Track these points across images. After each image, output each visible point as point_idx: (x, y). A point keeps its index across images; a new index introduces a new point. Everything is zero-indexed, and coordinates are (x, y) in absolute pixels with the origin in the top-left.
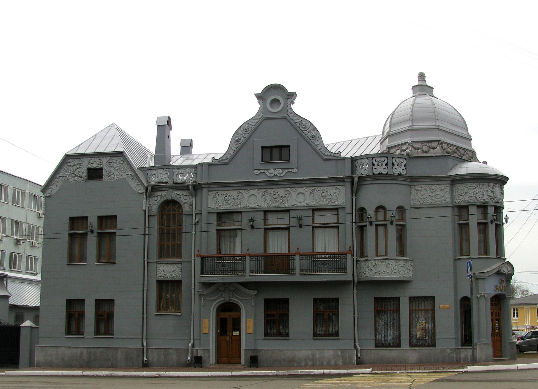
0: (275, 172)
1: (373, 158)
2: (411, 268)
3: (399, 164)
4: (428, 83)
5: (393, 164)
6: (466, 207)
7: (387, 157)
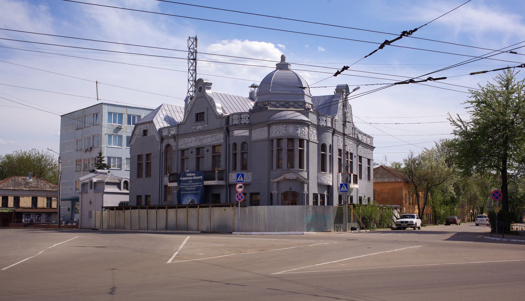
0: (199, 127)
2: (251, 177)
3: (245, 118)
4: (286, 61)
6: (282, 139)
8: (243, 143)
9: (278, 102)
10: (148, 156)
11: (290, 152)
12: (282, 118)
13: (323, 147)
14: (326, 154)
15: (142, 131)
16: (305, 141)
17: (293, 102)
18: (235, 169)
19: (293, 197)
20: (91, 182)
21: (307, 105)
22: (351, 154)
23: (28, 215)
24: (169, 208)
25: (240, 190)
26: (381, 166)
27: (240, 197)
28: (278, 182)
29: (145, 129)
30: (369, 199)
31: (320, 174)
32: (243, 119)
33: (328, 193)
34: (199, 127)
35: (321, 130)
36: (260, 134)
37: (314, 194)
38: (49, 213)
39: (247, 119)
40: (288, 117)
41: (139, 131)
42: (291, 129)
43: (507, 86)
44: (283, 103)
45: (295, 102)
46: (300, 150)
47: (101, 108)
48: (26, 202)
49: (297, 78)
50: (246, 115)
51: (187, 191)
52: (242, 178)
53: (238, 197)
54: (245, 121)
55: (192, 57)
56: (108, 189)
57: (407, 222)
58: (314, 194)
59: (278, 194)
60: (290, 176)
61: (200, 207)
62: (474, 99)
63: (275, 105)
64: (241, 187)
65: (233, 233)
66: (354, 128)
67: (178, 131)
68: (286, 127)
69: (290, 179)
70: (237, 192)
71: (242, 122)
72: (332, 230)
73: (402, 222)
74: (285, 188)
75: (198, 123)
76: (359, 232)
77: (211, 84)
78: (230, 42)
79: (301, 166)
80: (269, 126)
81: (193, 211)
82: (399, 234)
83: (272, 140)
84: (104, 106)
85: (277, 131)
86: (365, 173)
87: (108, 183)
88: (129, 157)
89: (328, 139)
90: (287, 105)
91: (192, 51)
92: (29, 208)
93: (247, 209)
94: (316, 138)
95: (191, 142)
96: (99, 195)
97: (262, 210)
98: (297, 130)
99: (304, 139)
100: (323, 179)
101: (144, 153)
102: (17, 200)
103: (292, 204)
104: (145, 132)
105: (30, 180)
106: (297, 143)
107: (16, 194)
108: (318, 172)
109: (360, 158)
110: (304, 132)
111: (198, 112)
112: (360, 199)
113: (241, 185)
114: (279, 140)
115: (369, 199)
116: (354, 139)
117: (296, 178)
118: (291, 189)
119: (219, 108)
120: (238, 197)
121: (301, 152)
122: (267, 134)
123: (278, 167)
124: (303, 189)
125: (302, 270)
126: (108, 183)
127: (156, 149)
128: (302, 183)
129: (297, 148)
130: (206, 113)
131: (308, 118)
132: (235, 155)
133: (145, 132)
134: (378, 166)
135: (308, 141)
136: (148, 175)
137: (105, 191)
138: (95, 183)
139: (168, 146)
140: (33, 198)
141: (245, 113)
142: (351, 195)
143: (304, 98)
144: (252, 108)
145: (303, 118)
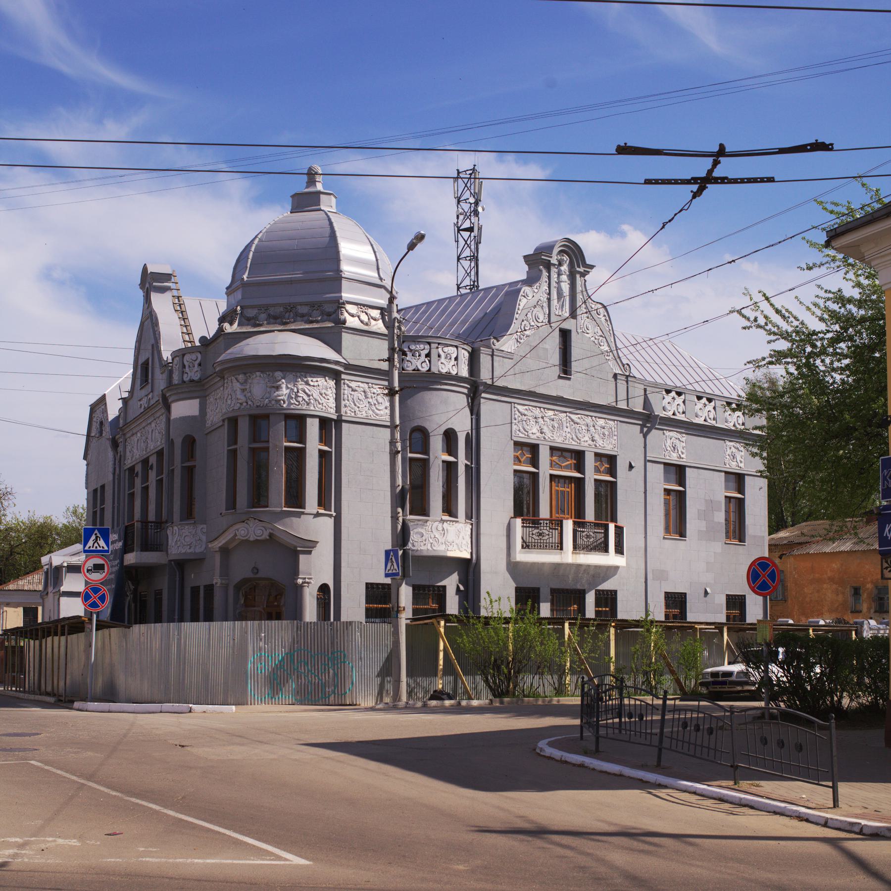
1: (184, 355)
5: (439, 356)
6: (266, 417)
7: (429, 343)
8: (190, 443)
9: (265, 308)
10: (103, 487)
14: (456, 464)
16: (313, 428)
17: (306, 304)
22: (609, 461)
32: (187, 370)
33: (463, 580)
35: (411, 387)
39: (196, 368)
42: (258, 386)
45: (312, 305)
49: (328, 229)
50: (194, 356)
52: (102, 543)
54: (193, 374)
55: (467, 225)
59: (226, 587)
60: (253, 531)
63: (255, 318)
68: (246, 381)
69: (247, 541)
71: (186, 378)
74: (241, 570)
78: (517, 162)
79: (296, 497)
86: (704, 515)
88: (85, 506)
90: (282, 317)
98: (278, 388)
103: (270, 617)
109: (678, 472)
110: (317, 396)
113: (99, 561)
116: (629, 414)
117: (265, 536)
118: (256, 570)
121: (297, 457)
123: (232, 504)
128: (293, 551)
129: (313, 445)
131: (338, 350)
135: (330, 427)
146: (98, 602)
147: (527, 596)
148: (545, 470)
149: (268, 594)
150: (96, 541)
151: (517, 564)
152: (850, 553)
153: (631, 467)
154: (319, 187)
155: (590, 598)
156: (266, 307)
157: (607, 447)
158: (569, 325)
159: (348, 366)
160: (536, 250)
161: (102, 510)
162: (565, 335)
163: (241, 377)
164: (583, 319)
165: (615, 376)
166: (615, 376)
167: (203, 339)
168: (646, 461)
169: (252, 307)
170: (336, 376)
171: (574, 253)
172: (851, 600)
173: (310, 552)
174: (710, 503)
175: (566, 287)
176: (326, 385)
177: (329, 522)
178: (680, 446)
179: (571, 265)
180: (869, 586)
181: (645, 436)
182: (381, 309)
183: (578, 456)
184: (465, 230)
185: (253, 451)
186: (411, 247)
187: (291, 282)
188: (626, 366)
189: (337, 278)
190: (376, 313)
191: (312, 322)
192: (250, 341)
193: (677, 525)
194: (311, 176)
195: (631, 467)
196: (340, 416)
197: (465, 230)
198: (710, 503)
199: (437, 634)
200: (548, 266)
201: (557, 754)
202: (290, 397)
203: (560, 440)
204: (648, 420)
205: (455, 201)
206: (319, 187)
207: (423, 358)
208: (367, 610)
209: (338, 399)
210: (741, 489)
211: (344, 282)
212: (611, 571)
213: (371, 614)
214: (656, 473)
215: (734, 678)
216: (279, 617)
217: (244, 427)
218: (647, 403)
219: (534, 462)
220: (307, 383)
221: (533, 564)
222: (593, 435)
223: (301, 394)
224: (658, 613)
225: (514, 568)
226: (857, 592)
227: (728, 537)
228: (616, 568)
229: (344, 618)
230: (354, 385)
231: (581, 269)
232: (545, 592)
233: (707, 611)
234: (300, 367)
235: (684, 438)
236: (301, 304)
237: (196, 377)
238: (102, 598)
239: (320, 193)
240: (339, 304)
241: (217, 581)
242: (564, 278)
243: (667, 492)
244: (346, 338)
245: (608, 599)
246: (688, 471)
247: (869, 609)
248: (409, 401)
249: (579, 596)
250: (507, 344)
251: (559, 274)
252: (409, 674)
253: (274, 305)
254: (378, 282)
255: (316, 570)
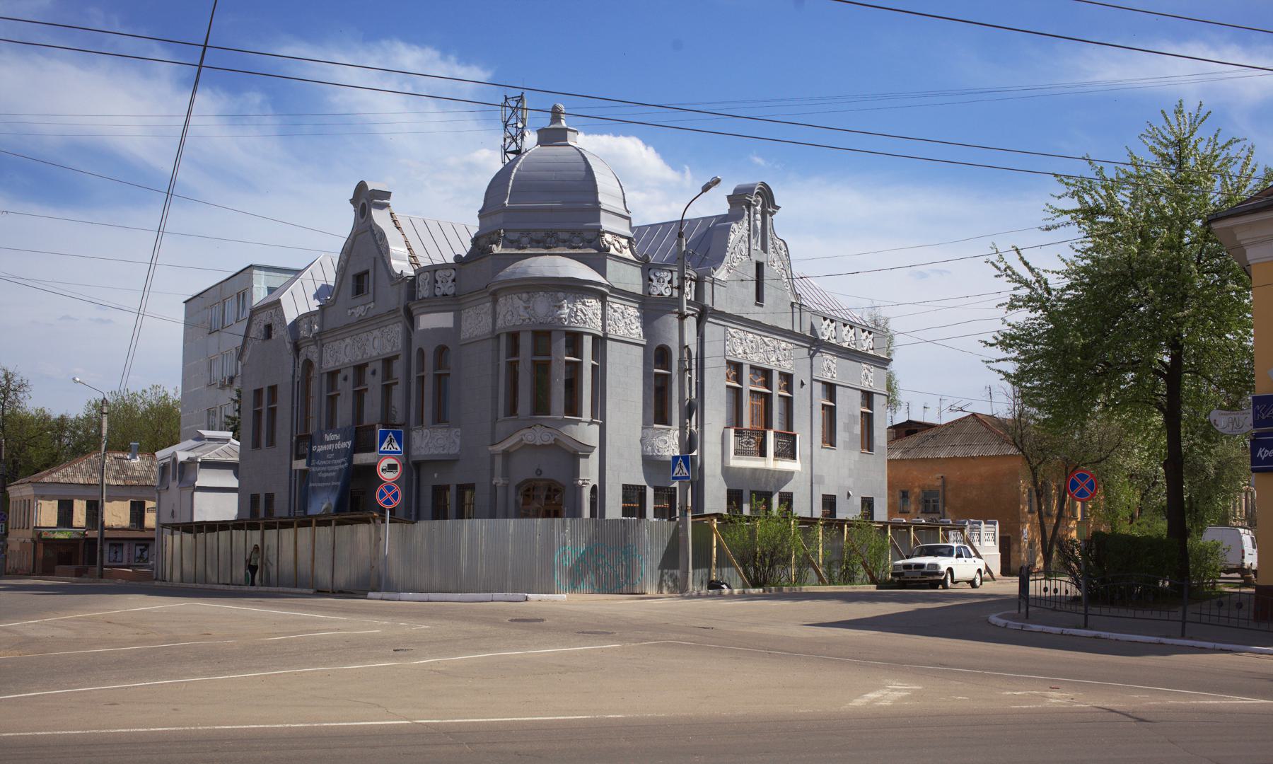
2: (458, 441)
8: (442, 351)
9: (526, 232)
10: (273, 389)
11: (547, 369)
12: (517, 276)
13: (659, 355)
15: (262, 327)
16: (587, 343)
17: (567, 231)
18: (420, 421)
19: (549, 495)
20: (175, 460)
21: (608, 237)
22: (787, 378)
23: (115, 545)
24: (299, 526)
25: (389, 476)
26: (974, 415)
27: (389, 496)
28: (507, 454)
29: (268, 321)
30: (868, 503)
31: (650, 432)
32: (439, 284)
34: (360, 311)
35: (651, 309)
36: (477, 322)
37: (627, 489)
38: (139, 543)
39: (450, 283)
40: (564, 273)
41: (258, 330)
42: (541, 305)
43: (1180, 161)
44: (540, 235)
45: (573, 233)
46: (568, 362)
47: (251, 280)
48: (117, 514)
51: (321, 480)
52: (396, 445)
53: (382, 495)
54: (448, 288)
55: (513, 147)
56: (205, 478)
57: (922, 566)
58: (627, 489)
59: (506, 487)
61: (339, 523)
62: (1074, 204)
63: (518, 241)
64: (392, 467)
65: (371, 594)
66: (797, 306)
67: (321, 325)
69: (534, 446)
70: (381, 481)
71: (438, 292)
72: (651, 591)
73: (907, 567)
74: (524, 470)
75: (359, 300)
76: (743, 596)
77: (387, 195)
79: (573, 407)
80: (495, 297)
81: (324, 533)
82: (807, 602)
83: (498, 337)
84: (255, 272)
85: (513, 312)
86: (848, 428)
87: (207, 465)
89: (680, 334)
90: (548, 241)
91: (513, 131)
92: (123, 529)
93: (423, 526)
94: (640, 330)
95: (341, 354)
96: (187, 493)
97: (475, 533)
98: (560, 307)
99: (582, 334)
100: (661, 445)
101: (265, 386)
102: (94, 510)
104: (269, 328)
105: (133, 461)
106: (560, 344)
107: (93, 494)
108: (646, 425)
109: (830, 389)
110: (587, 315)
111: (358, 270)
112: (829, 502)
113: (393, 462)
114: (514, 337)
115: (868, 503)
117: (551, 441)
118: (539, 472)
119: (399, 258)
120: (382, 495)
121: (574, 371)
122: (490, 320)
124: (576, 473)
125: (1215, 699)
126: (207, 465)
127: (284, 374)
128: (573, 455)
130: (371, 274)
131: (604, 275)
132: (421, 380)
133: (269, 328)
134: (960, 415)
135: (600, 342)
136: (271, 442)
137: (197, 484)
138: (182, 463)
139: (308, 364)
140: (60, 502)
141: (445, 266)
142: (785, 489)
143: (599, 220)
144: (464, 255)
145: (583, 272)
146: (392, 500)
147: (734, 497)
148: (747, 386)
149: (549, 495)
150: (390, 442)
151: (729, 468)
152: (901, 460)
153: (802, 384)
154: (564, 124)
155: (775, 500)
156: (528, 232)
157: (787, 367)
158: (762, 258)
159: (613, 289)
160: (735, 190)
161: (272, 411)
162: (759, 266)
163: (525, 296)
164: (772, 255)
165: (792, 304)
166: (792, 304)
167: (458, 257)
168: (812, 380)
169: (515, 231)
170: (602, 297)
171: (766, 194)
172: (899, 501)
173: (587, 457)
174: (852, 416)
175: (759, 224)
176: (594, 304)
177: (596, 428)
178: (833, 366)
179: (763, 206)
180: (917, 490)
181: (812, 357)
182: (628, 238)
183: (767, 373)
184: (512, 152)
185: (535, 364)
186: (706, 188)
187: (551, 210)
188: (798, 296)
189: (596, 209)
190: (624, 242)
191: (574, 248)
192: (526, 262)
193: (830, 439)
194: (556, 114)
195: (802, 384)
196: (605, 334)
197: (512, 152)
198: (852, 416)
199: (711, 530)
200: (749, 205)
201: (1002, 622)
202: (570, 316)
203: (756, 359)
204: (815, 344)
205: (501, 126)
206: (564, 124)
207: (666, 284)
208: (624, 508)
209: (604, 319)
210: (870, 406)
211: (602, 213)
212: (788, 476)
213: (626, 512)
214: (818, 388)
215: (925, 569)
216: (557, 514)
217: (526, 343)
218: (813, 329)
219: (738, 378)
220: (584, 304)
221: (740, 469)
222: (780, 356)
223: (579, 313)
224: (818, 513)
225: (727, 472)
226: (905, 495)
227: (863, 447)
228: (792, 473)
229: (608, 517)
230: (616, 305)
231: (771, 210)
232: (746, 494)
233: (848, 511)
234: (578, 289)
235: (835, 360)
236: (562, 231)
237: (451, 291)
238: (395, 496)
239: (566, 130)
240: (599, 233)
241: (499, 481)
242: (759, 216)
243: (824, 406)
244: (610, 264)
245: (787, 499)
246: (838, 388)
247: (916, 510)
248: (655, 323)
249: (768, 496)
250: (721, 274)
251: (755, 214)
252: (694, 568)
253: (535, 231)
254: (625, 214)
255: (589, 472)
